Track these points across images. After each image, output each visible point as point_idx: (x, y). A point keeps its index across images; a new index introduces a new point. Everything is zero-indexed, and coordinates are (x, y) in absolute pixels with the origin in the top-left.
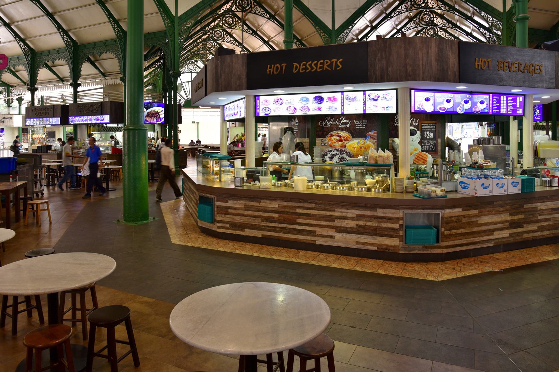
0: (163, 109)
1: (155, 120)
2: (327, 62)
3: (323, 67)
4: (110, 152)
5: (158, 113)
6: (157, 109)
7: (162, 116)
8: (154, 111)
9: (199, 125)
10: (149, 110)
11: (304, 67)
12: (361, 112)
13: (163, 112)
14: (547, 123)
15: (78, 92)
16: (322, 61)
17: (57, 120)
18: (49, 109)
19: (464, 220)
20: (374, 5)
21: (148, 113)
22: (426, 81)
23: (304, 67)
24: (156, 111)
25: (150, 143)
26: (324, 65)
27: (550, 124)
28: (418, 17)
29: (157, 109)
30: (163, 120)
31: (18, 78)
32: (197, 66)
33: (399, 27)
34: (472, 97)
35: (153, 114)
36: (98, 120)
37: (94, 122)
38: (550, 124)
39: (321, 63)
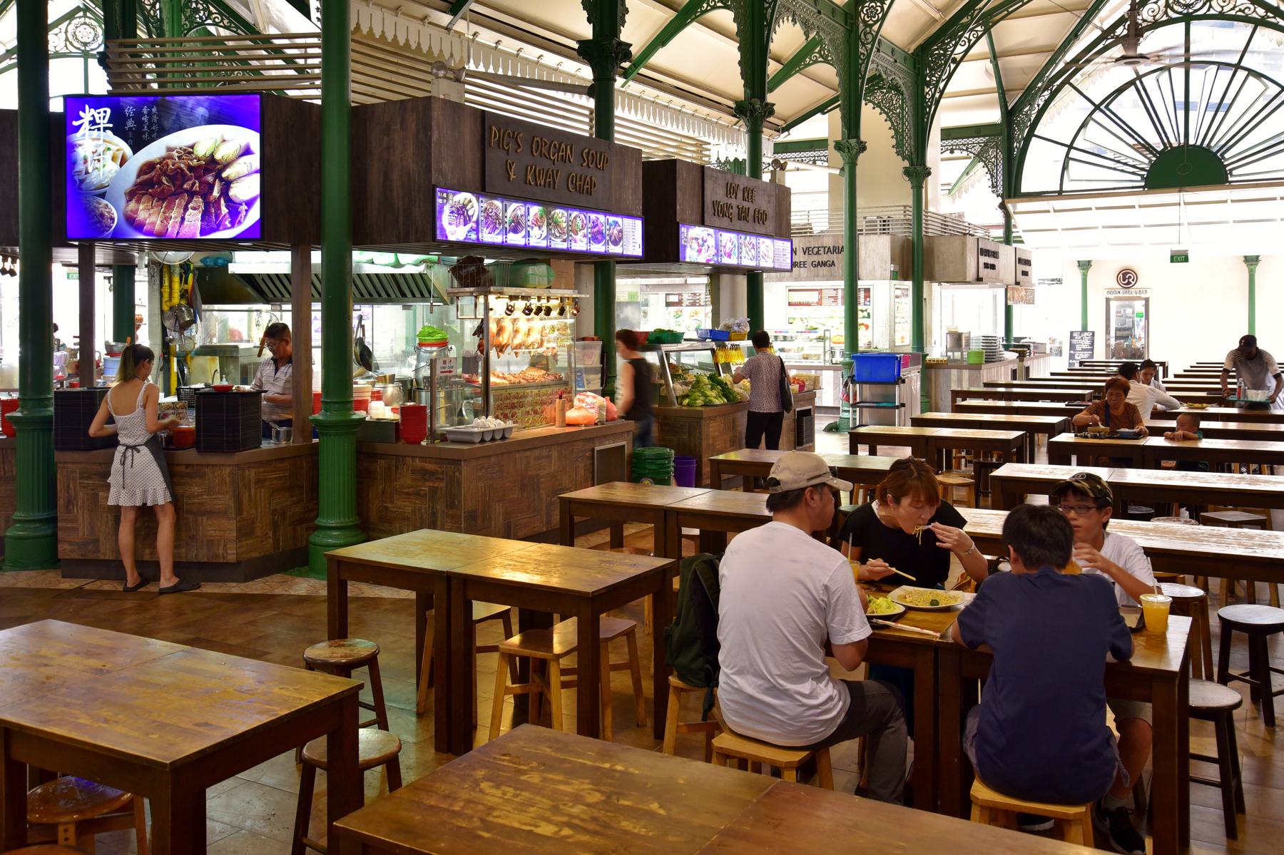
4: (909, 284)
5: (213, 166)
6: (206, 139)
7: (247, 187)
8: (189, 151)
9: (1260, 270)
10: (155, 151)
12: (82, 92)
13: (254, 161)
14: (301, 261)
15: (590, 92)
17: (631, 236)
18: (722, 211)
19: (449, 437)
21: (148, 167)
22: (878, 798)
24: (201, 151)
27: (316, 257)
29: (206, 139)
30: (254, 215)
32: (1171, 21)
34: (1269, 515)
35: (178, 177)
36: (596, 237)
37: (580, 244)
38: (316, 257)
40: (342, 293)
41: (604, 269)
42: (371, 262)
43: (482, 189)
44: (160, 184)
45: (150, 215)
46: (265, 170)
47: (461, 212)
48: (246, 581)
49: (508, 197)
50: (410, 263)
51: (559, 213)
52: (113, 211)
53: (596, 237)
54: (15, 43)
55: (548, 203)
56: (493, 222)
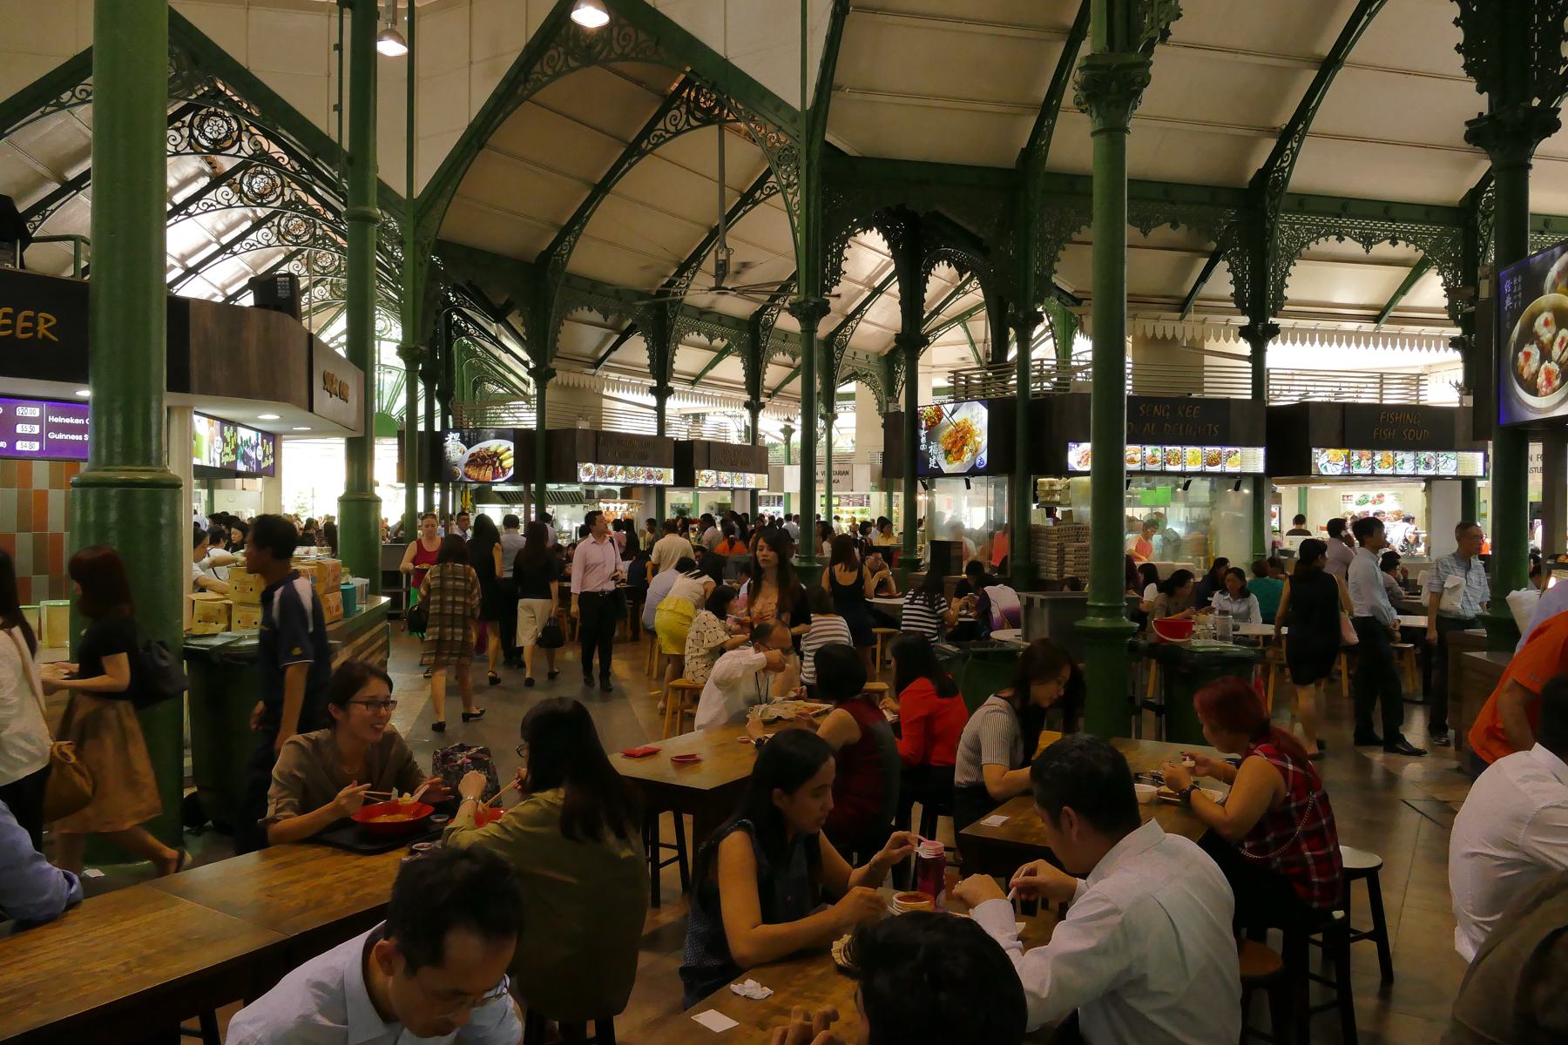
0: (511, 445)
1: (489, 473)
2: (47, 321)
3: (34, 330)
5: (496, 455)
6: (493, 445)
7: (509, 462)
10: (475, 449)
11: (29, 324)
14: (528, 488)
16: (31, 313)
17: (668, 476)
20: (37, 113)
23: (29, 324)
24: (492, 449)
25: (245, 501)
26: (36, 324)
28: (276, 221)
29: (493, 445)
30: (511, 472)
31: (952, 321)
33: (225, 240)
35: (483, 458)
36: (650, 477)
37: (641, 481)
39: (27, 319)
40: (541, 499)
41: (661, 490)
42: (552, 487)
43: (596, 461)
44: (477, 461)
45: (473, 472)
46: (515, 455)
47: (588, 471)
48: (515, 564)
49: (607, 463)
50: (52, 436)
51: (631, 468)
52: (460, 471)
53: (650, 477)
54: (169, 231)
55: (626, 465)
56: (600, 473)
